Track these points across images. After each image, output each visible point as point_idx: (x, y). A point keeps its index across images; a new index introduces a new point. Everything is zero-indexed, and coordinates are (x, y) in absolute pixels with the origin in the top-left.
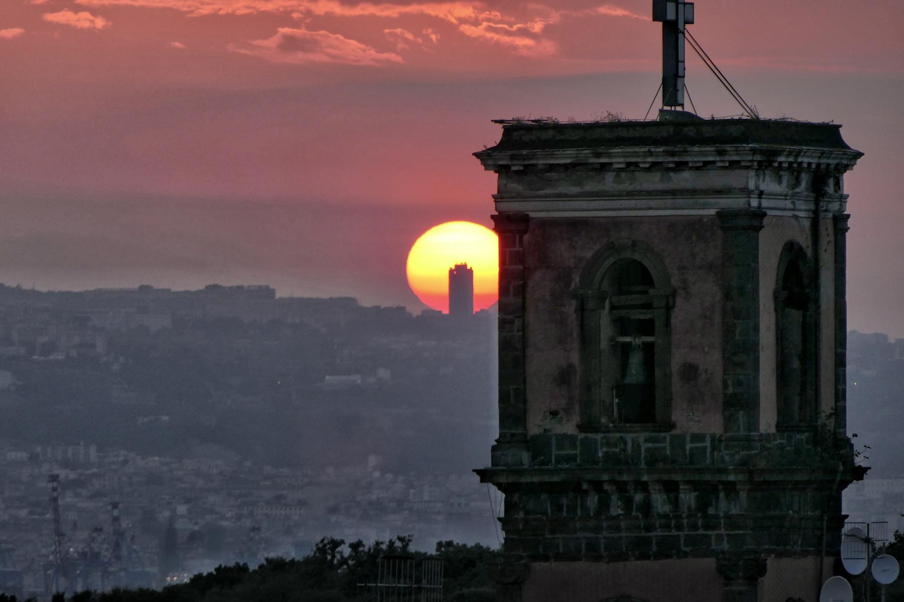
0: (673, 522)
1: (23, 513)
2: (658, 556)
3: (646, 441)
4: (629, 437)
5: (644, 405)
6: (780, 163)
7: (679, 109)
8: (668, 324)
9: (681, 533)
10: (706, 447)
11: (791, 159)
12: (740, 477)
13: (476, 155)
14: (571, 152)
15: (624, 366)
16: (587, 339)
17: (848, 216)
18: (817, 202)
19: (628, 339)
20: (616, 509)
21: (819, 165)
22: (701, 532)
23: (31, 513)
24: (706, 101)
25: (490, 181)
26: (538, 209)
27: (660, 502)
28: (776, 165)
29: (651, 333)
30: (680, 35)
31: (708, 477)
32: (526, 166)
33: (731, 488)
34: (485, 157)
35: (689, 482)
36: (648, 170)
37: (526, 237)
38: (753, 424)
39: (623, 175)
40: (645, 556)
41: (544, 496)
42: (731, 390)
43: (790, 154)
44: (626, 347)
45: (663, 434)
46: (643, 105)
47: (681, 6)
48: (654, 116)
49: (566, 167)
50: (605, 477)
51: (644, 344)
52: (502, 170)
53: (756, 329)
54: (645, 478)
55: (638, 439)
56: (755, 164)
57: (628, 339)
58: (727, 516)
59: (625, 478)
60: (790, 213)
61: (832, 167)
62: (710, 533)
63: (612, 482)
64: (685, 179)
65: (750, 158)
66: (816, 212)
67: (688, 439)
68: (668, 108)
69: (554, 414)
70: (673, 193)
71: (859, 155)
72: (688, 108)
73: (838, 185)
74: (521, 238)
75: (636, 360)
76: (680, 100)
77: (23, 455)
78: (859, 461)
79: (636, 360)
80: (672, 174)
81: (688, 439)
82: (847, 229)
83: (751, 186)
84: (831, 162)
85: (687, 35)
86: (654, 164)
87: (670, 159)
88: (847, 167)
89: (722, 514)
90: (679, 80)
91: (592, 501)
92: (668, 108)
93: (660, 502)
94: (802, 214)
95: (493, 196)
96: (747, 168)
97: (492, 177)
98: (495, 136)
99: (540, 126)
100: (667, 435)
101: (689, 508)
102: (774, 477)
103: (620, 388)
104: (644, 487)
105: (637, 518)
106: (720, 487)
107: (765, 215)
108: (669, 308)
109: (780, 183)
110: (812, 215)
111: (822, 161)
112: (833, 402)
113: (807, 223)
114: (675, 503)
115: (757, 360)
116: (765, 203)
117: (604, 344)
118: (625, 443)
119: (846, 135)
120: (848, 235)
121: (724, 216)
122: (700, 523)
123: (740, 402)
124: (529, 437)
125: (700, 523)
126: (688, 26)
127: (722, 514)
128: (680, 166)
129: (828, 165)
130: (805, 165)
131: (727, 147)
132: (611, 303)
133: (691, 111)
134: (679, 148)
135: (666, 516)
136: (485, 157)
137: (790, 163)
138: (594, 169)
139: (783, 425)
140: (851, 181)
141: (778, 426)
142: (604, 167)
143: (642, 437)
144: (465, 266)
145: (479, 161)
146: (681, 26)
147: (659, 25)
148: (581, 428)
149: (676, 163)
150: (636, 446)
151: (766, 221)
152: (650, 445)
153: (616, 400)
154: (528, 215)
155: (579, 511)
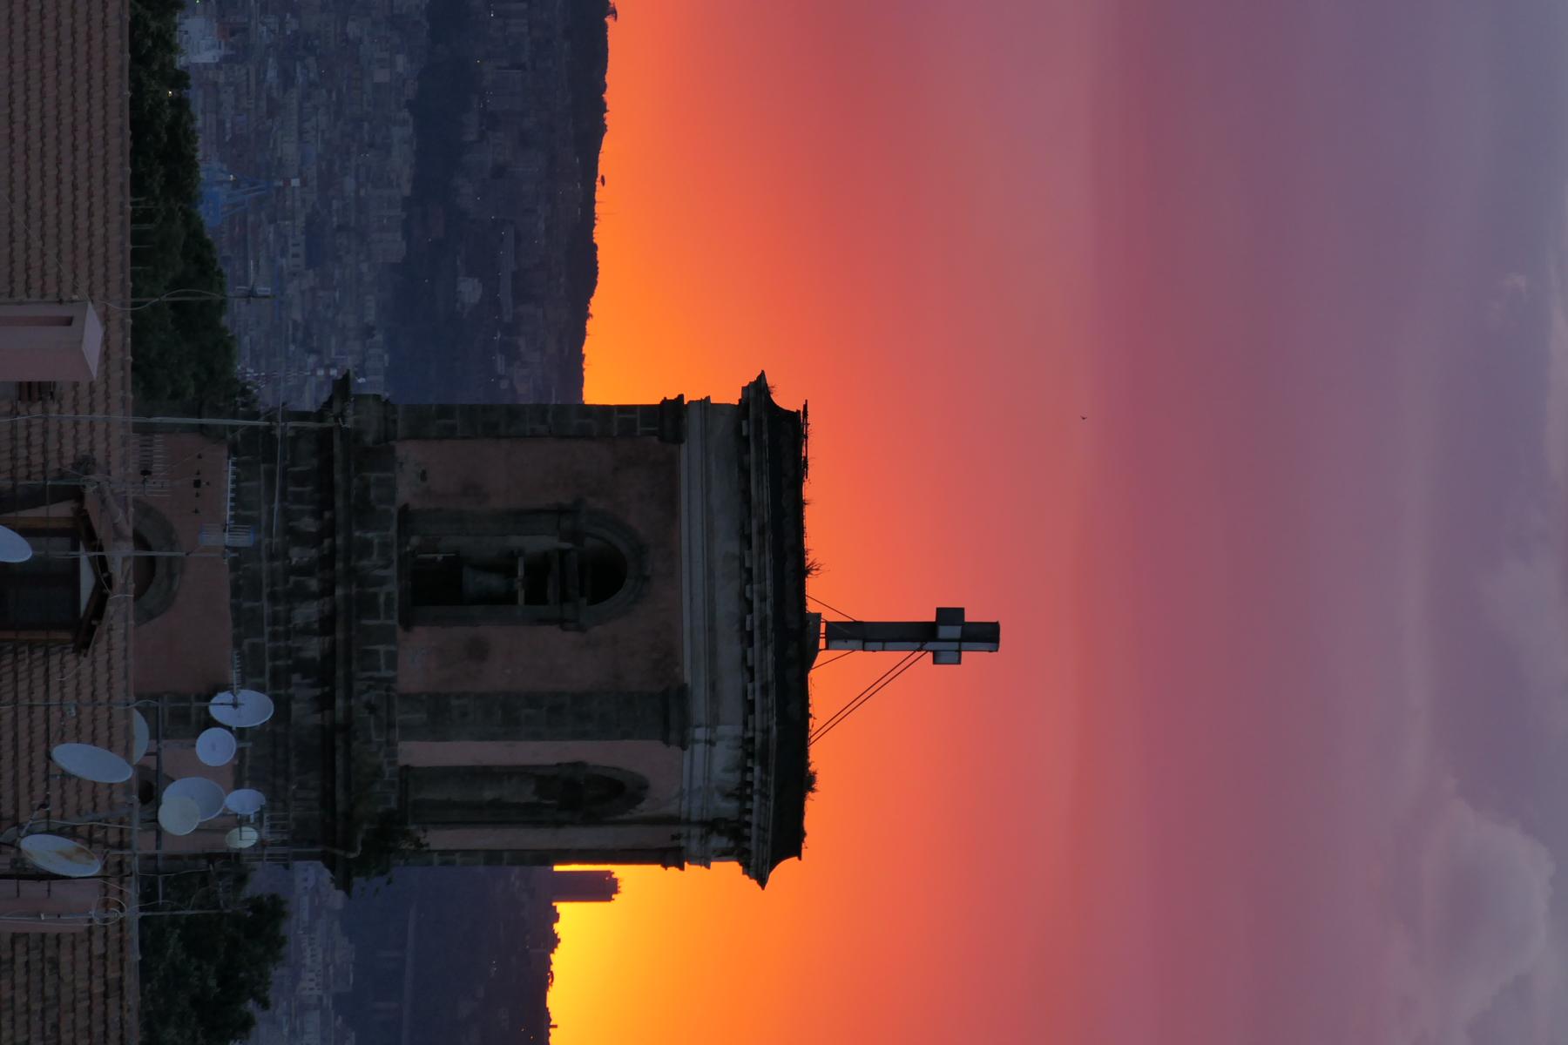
0: (281, 628)
1: (297, 315)
2: (236, 609)
3: (388, 594)
4: (392, 572)
5: (437, 588)
6: (751, 770)
7: (822, 643)
8: (542, 621)
9: (266, 637)
10: (378, 669)
11: (756, 786)
12: (340, 715)
13: (762, 376)
14: (766, 495)
15: (487, 568)
16: (522, 518)
17: (682, 868)
18: (702, 823)
19: (521, 572)
20: (297, 555)
21: (749, 825)
22: (268, 665)
23: (295, 324)
24: (832, 678)
25: (728, 394)
26: (690, 455)
27: (307, 612)
28: (749, 764)
29: (528, 601)
30: (918, 645)
31: (340, 673)
32: (747, 439)
33: (325, 703)
34: (758, 390)
35: (333, 644)
36: (742, 594)
37: (655, 439)
38: (410, 732)
39: (736, 564)
40: (236, 591)
41: (315, 462)
42: (455, 702)
43: (764, 783)
44: (510, 572)
45: (396, 615)
46: (829, 594)
47: (955, 646)
48: (812, 607)
49: (746, 492)
50: (339, 541)
51: (515, 594)
52: (744, 405)
53: (537, 736)
54: (339, 592)
55: (391, 588)
56: (750, 734)
57: (521, 572)
58: (290, 698)
59: (339, 566)
60: (686, 786)
61: (746, 845)
62: (267, 676)
63: (333, 549)
64: (730, 651)
65: (758, 726)
66: (688, 822)
67: (392, 648)
68: (823, 630)
69: (423, 476)
70: (711, 630)
71: (762, 882)
72: (822, 657)
73: (724, 855)
74: (653, 434)
75: (494, 582)
76: (834, 644)
77: (371, 317)
78: (358, 882)
79: (494, 582)
80: (737, 627)
81: (392, 648)
82: (665, 866)
83: (722, 729)
84: (753, 841)
85: (918, 654)
86: (750, 603)
87: (756, 623)
88: (747, 869)
89: (291, 691)
90: (859, 643)
91: (308, 524)
92: (823, 630)
93: (307, 612)
94: (685, 803)
95: (708, 398)
96: (745, 724)
97: (733, 397)
98: (785, 400)
99: (799, 468)
100: (395, 622)
101: (299, 649)
102: (339, 762)
103: (456, 563)
104: (327, 590)
105: (287, 582)
106: (327, 689)
107: (683, 746)
108: (562, 622)
109: (726, 770)
110: (684, 816)
111: (754, 828)
112: (441, 847)
113: (672, 809)
114: (306, 631)
115: (493, 737)
116: (699, 748)
117: (515, 541)
118: (385, 567)
119: (787, 867)
120: (658, 868)
121: (683, 692)
122: (280, 663)
123: (440, 715)
124: (392, 443)
125: (280, 663)
126: (930, 655)
127: (291, 691)
128: (747, 638)
129: (749, 839)
130: (748, 805)
131: (772, 696)
132: (568, 551)
133: (817, 662)
134: (770, 635)
135: (289, 620)
136: (758, 390)
137: (751, 784)
138: (742, 527)
139: (408, 774)
140: (728, 871)
141: (407, 768)
142: (746, 539)
143: (393, 588)
144: (616, 892)
145: (754, 379)
146: (929, 645)
147: (931, 617)
148: (404, 511)
149: (751, 634)
150: (381, 581)
151: (675, 749)
152: (382, 599)
153: (440, 557)
154: (682, 441)
155: (295, 507)
